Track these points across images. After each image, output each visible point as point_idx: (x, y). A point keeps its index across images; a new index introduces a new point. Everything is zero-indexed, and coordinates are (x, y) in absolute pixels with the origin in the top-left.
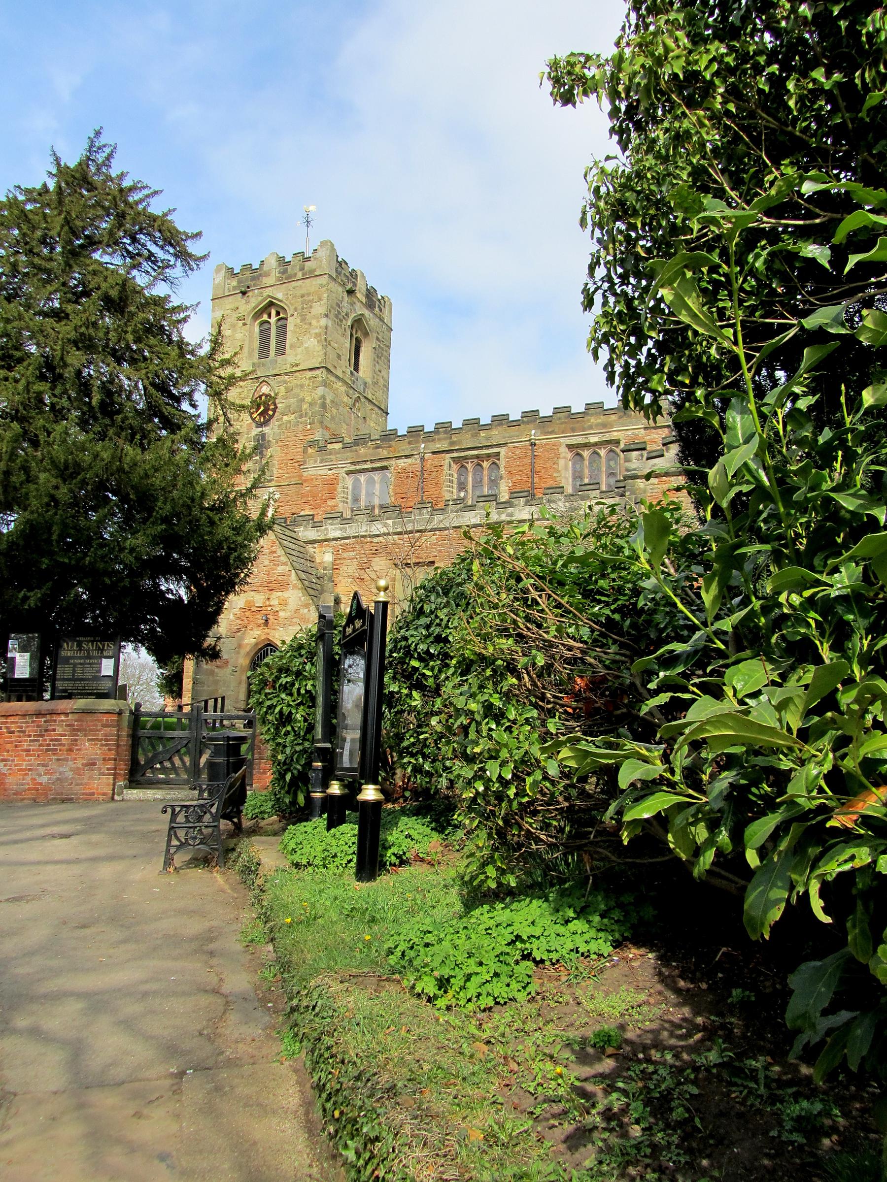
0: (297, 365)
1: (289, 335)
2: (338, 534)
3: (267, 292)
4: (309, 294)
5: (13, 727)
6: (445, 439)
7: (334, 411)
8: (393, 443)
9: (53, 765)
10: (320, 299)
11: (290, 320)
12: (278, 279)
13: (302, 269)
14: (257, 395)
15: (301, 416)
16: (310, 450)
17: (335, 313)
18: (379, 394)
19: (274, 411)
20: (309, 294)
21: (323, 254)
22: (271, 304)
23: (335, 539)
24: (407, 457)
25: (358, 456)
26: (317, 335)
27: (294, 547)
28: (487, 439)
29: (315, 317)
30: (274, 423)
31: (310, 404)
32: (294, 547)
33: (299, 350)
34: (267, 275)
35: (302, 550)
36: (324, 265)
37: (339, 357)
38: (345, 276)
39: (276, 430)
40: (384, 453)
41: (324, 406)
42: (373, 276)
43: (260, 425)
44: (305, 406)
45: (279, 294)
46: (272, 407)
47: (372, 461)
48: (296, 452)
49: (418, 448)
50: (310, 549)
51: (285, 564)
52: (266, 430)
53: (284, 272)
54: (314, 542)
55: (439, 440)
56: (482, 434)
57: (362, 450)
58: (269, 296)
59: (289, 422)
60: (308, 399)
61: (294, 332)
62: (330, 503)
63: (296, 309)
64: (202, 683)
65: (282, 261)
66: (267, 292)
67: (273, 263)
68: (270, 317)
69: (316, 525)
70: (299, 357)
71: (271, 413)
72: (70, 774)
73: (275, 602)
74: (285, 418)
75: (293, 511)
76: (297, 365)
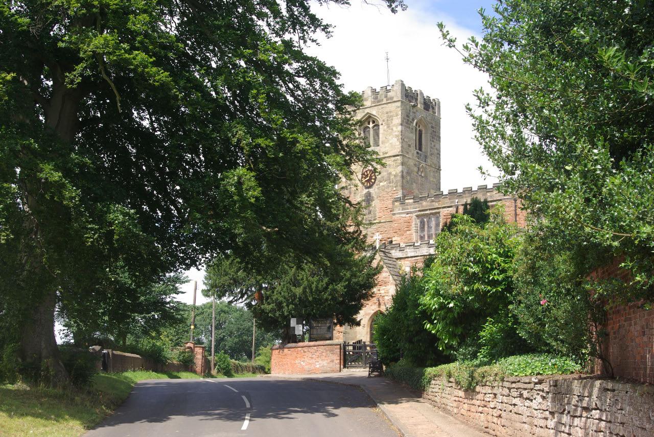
0: (386, 153)
1: (381, 136)
2: (413, 254)
3: (367, 111)
4: (391, 112)
5: (306, 350)
6: (469, 197)
7: (408, 178)
8: (441, 199)
9: (320, 362)
10: (397, 115)
11: (381, 127)
12: (373, 102)
13: (386, 97)
14: (364, 171)
15: (390, 183)
16: (396, 204)
17: (407, 121)
18: (435, 161)
19: (375, 179)
20: (391, 112)
21: (398, 88)
22: (370, 117)
23: (412, 257)
24: (449, 207)
25: (422, 206)
26: (397, 136)
27: (390, 262)
28: (491, 197)
29: (394, 125)
30: (375, 186)
31: (395, 176)
32: (390, 262)
33: (387, 145)
34: (366, 100)
35: (394, 263)
36: (396, 94)
37: (409, 146)
38: (409, 95)
39: (376, 190)
40: (436, 205)
41: (403, 177)
42: (430, 92)
43: (367, 188)
44: (392, 177)
45: (374, 112)
46: (374, 177)
47: (430, 209)
48: (389, 203)
49: (454, 202)
50: (399, 262)
51: (386, 272)
52: (371, 190)
53: (376, 98)
54: (401, 258)
55: (466, 197)
56: (488, 194)
57: (424, 203)
58: (368, 113)
59: (384, 186)
60: (394, 173)
61: (383, 134)
62: (408, 232)
63: (384, 121)
64: (349, 333)
65: (374, 91)
66: (367, 111)
67: (369, 93)
68: (369, 124)
69: (402, 250)
70: (387, 149)
71: (373, 181)
72: (326, 364)
73: (382, 292)
74: (381, 184)
75: (388, 236)
76: (386, 153)
